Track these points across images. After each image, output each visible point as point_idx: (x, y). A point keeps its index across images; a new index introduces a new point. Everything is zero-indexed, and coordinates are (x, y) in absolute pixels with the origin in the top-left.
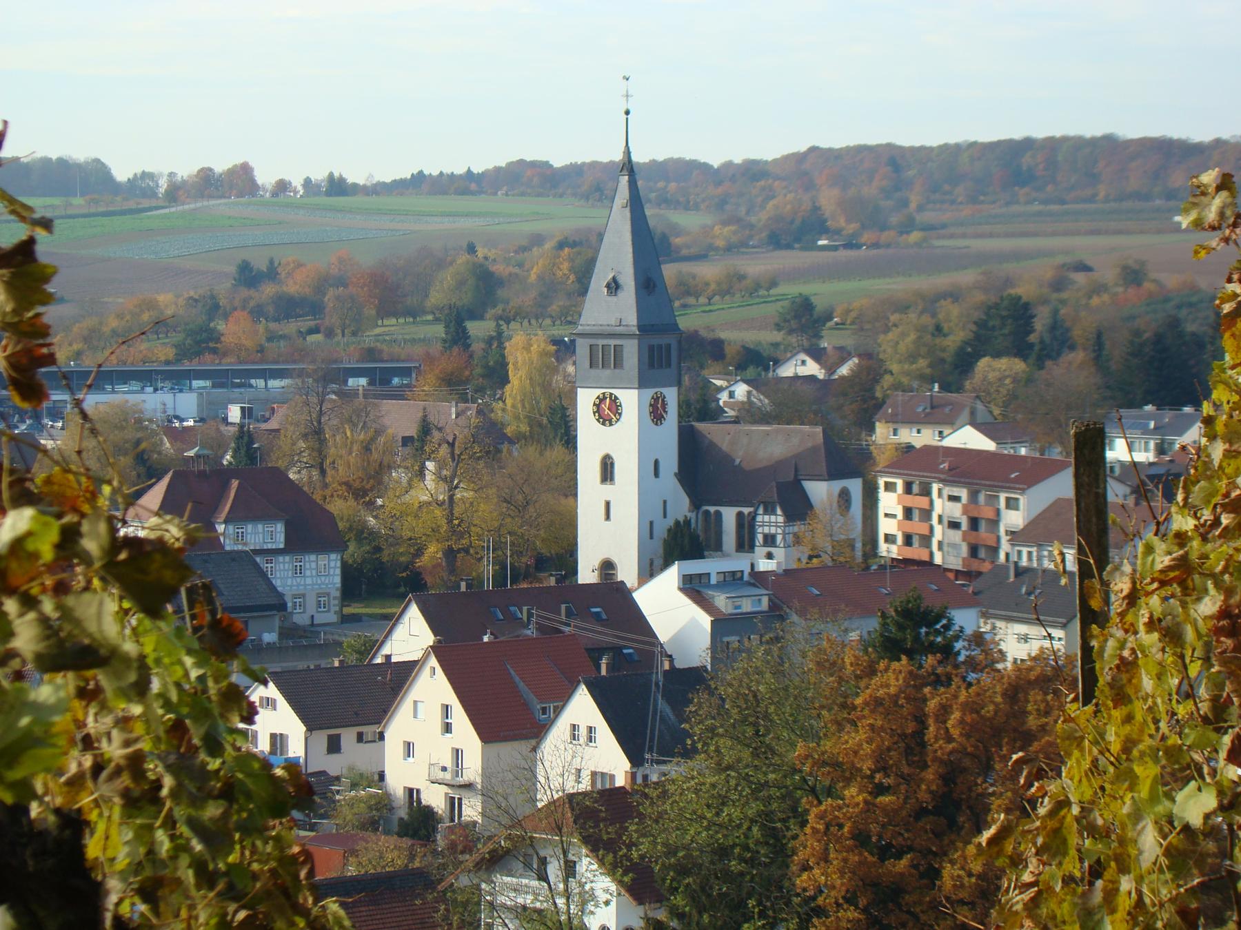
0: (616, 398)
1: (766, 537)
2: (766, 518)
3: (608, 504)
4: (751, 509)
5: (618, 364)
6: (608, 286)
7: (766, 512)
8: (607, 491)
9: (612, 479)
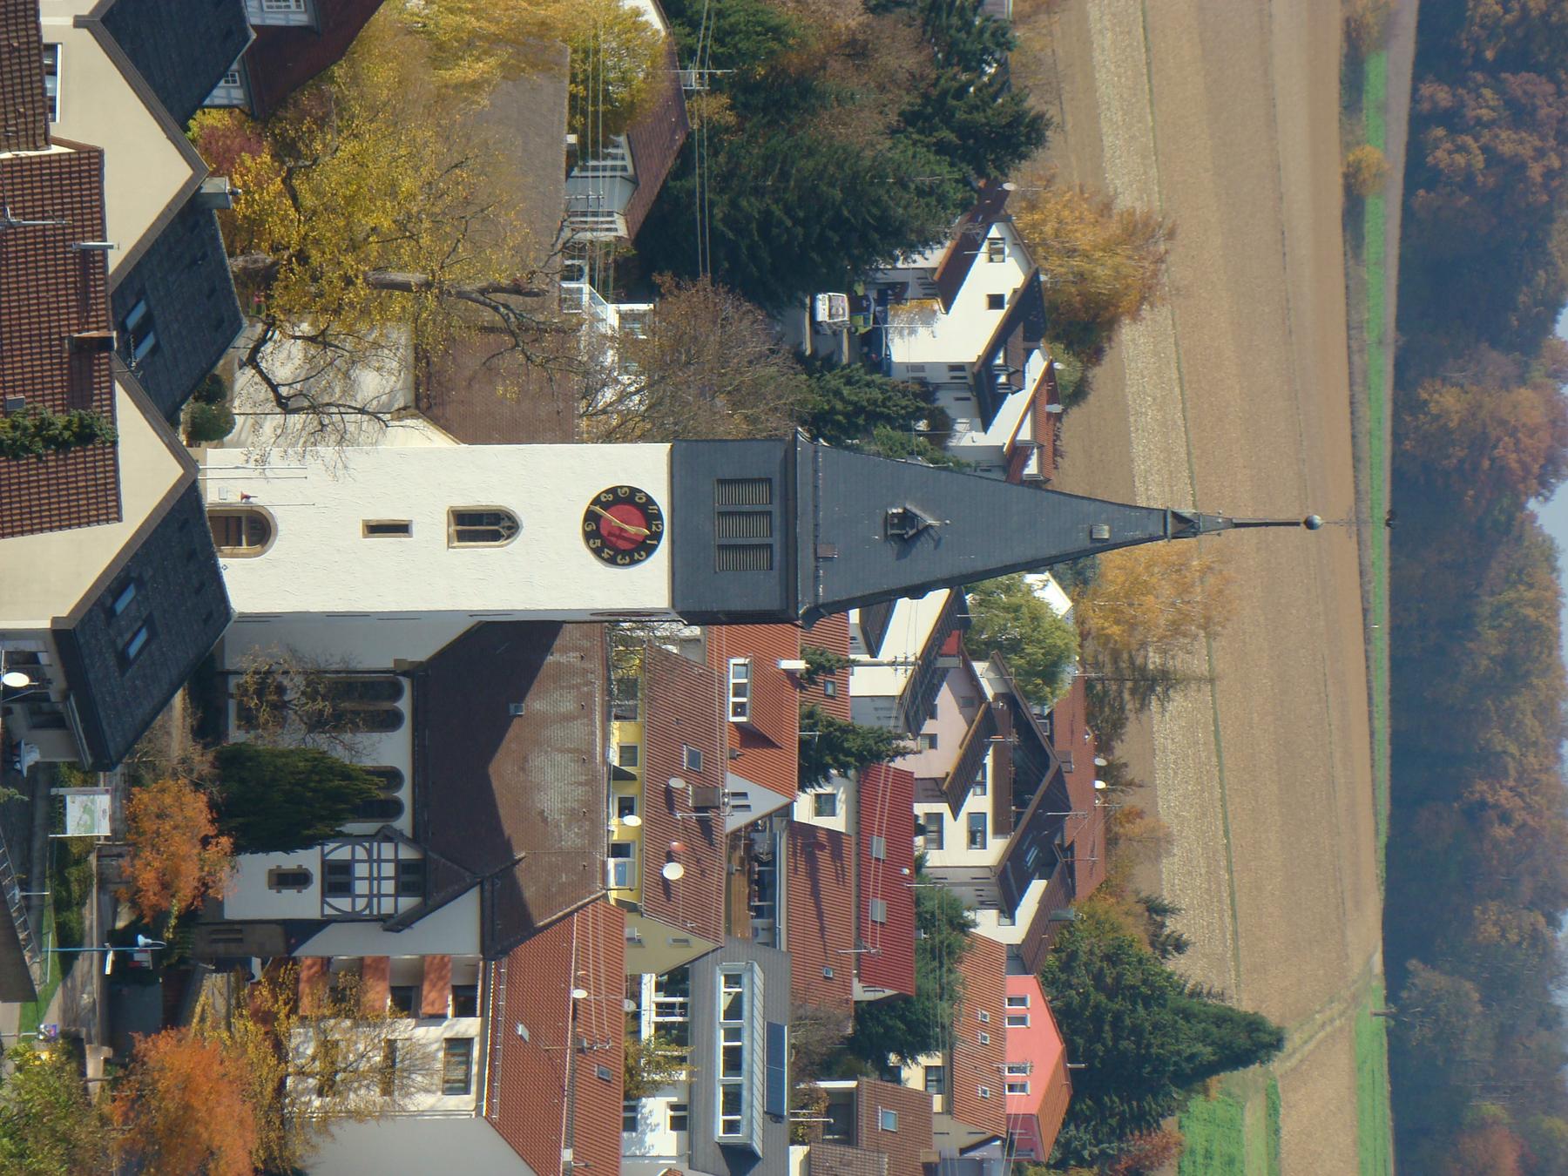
0: (650, 550)
1: (345, 868)
2: (389, 870)
3: (401, 528)
4: (408, 832)
6: (907, 518)
7: (403, 867)
8: (433, 527)
9: (462, 536)
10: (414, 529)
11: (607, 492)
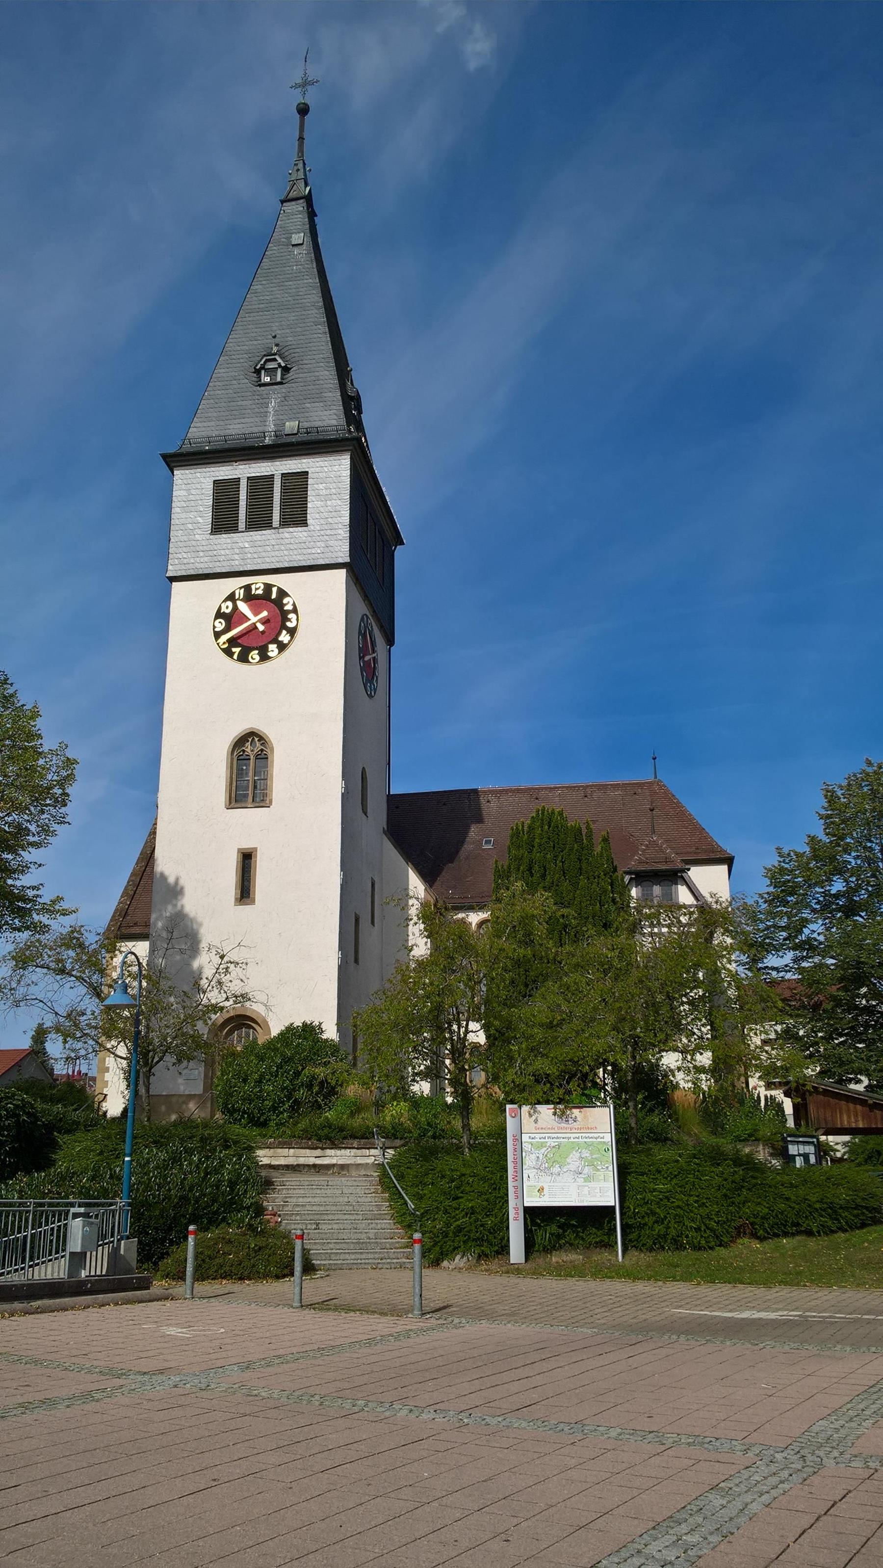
0: (282, 594)
3: (247, 858)
5: (296, 514)
8: (248, 826)
10: (247, 845)
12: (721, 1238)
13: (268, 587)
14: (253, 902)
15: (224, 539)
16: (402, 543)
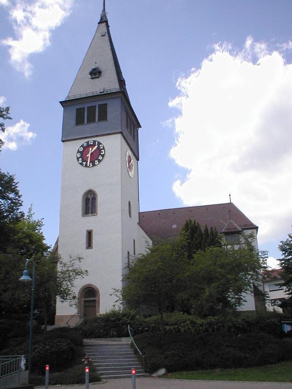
0: (99, 143)
3: (90, 234)
5: (103, 117)
8: (90, 222)
10: (90, 229)
11: (78, 160)
12: (213, 366)
13: (94, 142)
14: (92, 248)
15: (79, 127)
16: (141, 127)
